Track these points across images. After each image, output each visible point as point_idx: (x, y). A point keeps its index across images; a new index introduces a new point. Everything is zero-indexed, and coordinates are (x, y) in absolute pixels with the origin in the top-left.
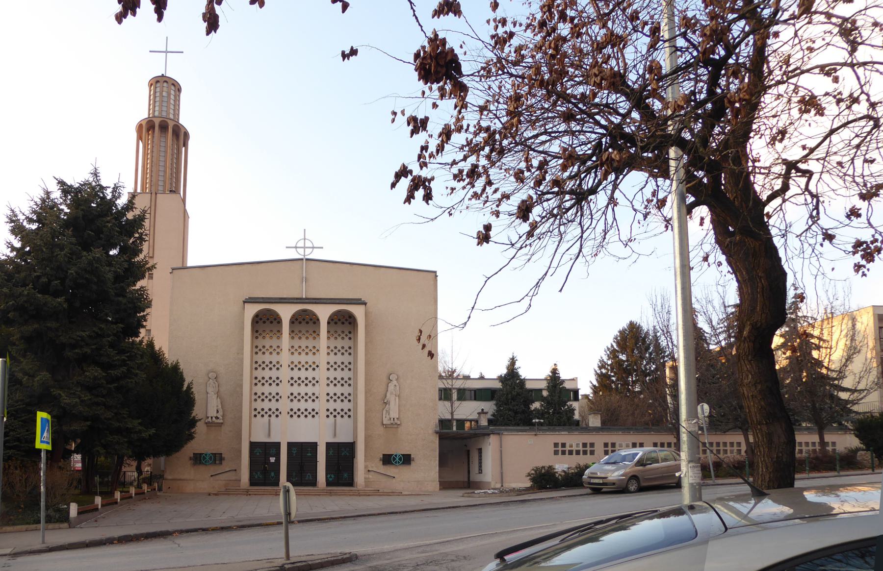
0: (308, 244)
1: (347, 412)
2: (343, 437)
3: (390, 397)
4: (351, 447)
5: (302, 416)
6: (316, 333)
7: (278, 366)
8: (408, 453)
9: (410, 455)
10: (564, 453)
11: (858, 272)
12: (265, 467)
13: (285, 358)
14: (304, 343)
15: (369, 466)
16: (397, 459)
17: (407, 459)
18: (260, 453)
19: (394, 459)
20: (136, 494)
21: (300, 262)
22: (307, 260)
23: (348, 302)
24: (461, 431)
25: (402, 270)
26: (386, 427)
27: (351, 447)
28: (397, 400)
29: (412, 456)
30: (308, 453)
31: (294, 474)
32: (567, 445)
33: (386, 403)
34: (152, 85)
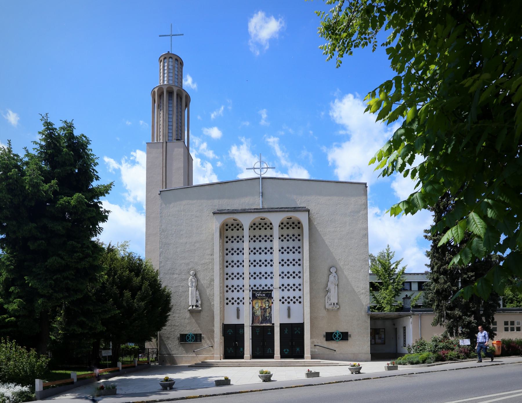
1: (298, 299)
2: (294, 320)
3: (332, 287)
4: (301, 326)
8: (346, 331)
10: (512, 330)
12: (235, 343)
15: (315, 341)
16: (337, 336)
17: (345, 336)
18: (231, 333)
19: (335, 336)
20: (123, 368)
21: (257, 180)
22: (263, 178)
27: (301, 326)
28: (336, 288)
29: (349, 334)
30: (268, 332)
31: (258, 349)
32: (516, 323)
33: (328, 291)
34: (161, 61)
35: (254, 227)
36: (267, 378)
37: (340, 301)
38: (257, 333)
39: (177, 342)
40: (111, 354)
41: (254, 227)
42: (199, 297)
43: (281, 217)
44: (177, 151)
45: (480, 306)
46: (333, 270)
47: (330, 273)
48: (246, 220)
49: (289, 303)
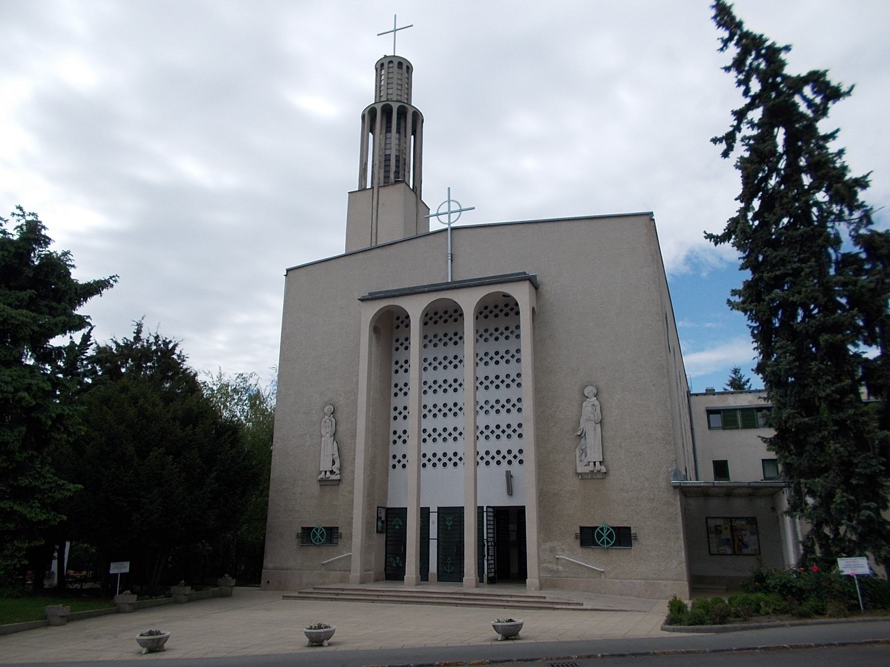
0: (454, 207)
5: (440, 465)
6: (457, 338)
7: (456, 385)
8: (625, 525)
9: (630, 528)
11: (113, 285)
13: (467, 372)
14: (440, 352)
16: (605, 537)
19: (600, 536)
21: (444, 234)
22: (453, 229)
23: (503, 279)
24: (723, 482)
25: (595, 221)
26: (582, 479)
35: (486, 312)
36: (510, 633)
37: (608, 457)
38: (448, 526)
39: (294, 543)
40: (127, 570)
41: (486, 312)
42: (337, 455)
43: (424, 301)
44: (393, 196)
45: (801, 478)
46: (589, 391)
47: (584, 398)
48: (415, 307)
49: (510, 462)
